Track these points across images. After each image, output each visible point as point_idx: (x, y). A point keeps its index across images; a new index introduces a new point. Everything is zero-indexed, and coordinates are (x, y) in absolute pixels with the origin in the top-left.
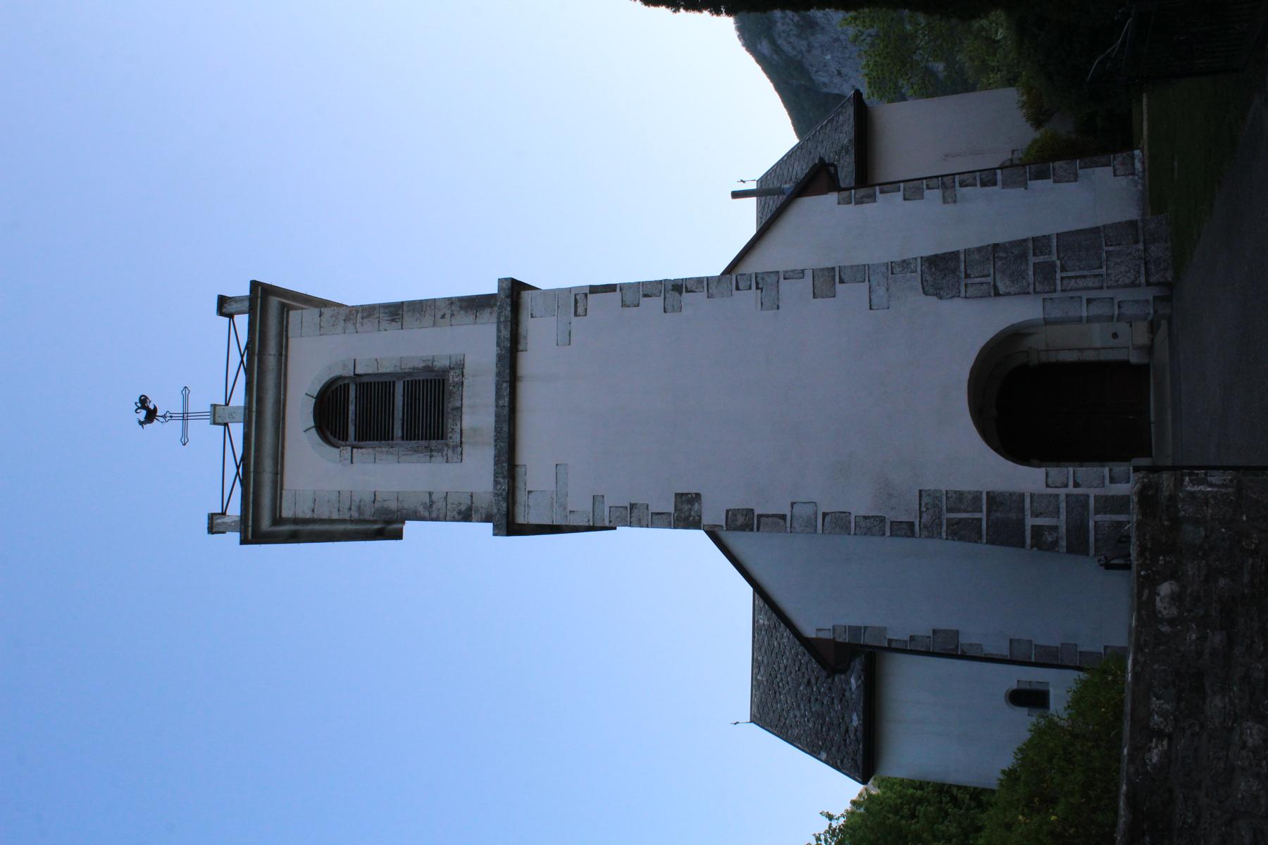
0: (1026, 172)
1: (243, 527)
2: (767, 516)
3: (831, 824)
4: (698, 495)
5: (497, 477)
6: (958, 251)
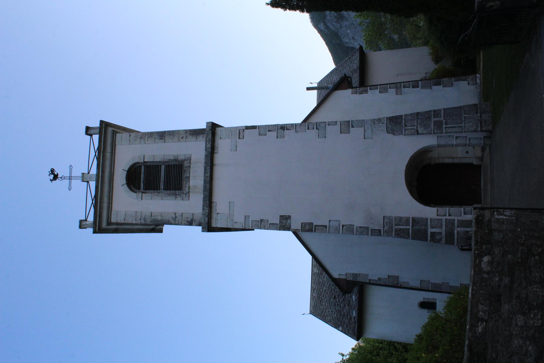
1: (94, 226)
2: (319, 226)
3: (343, 358)
4: (290, 216)
6: (402, 115)
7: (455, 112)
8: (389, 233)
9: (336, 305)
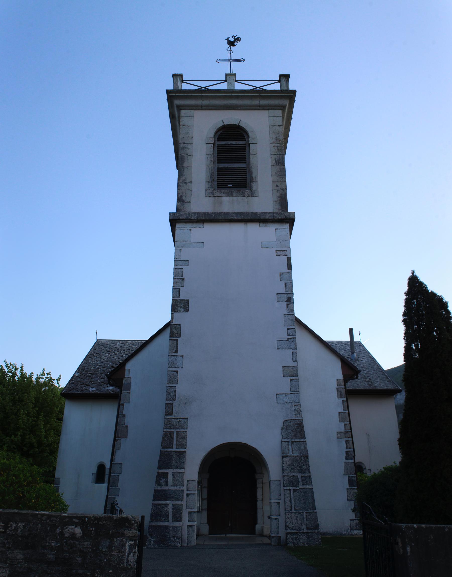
0: (352, 474)
1: (175, 91)
2: (177, 344)
3: (55, 380)
4: (187, 311)
5: (197, 214)
6: (305, 438)
7: (309, 502)
8: (168, 424)
9: (104, 369)
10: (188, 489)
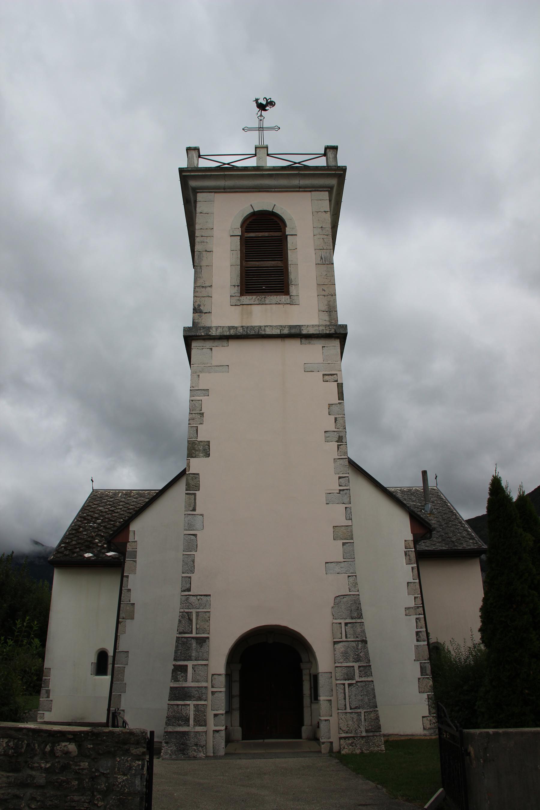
1: (190, 169)
2: (195, 499)
4: (208, 455)
8: (186, 603)
10: (213, 685)
